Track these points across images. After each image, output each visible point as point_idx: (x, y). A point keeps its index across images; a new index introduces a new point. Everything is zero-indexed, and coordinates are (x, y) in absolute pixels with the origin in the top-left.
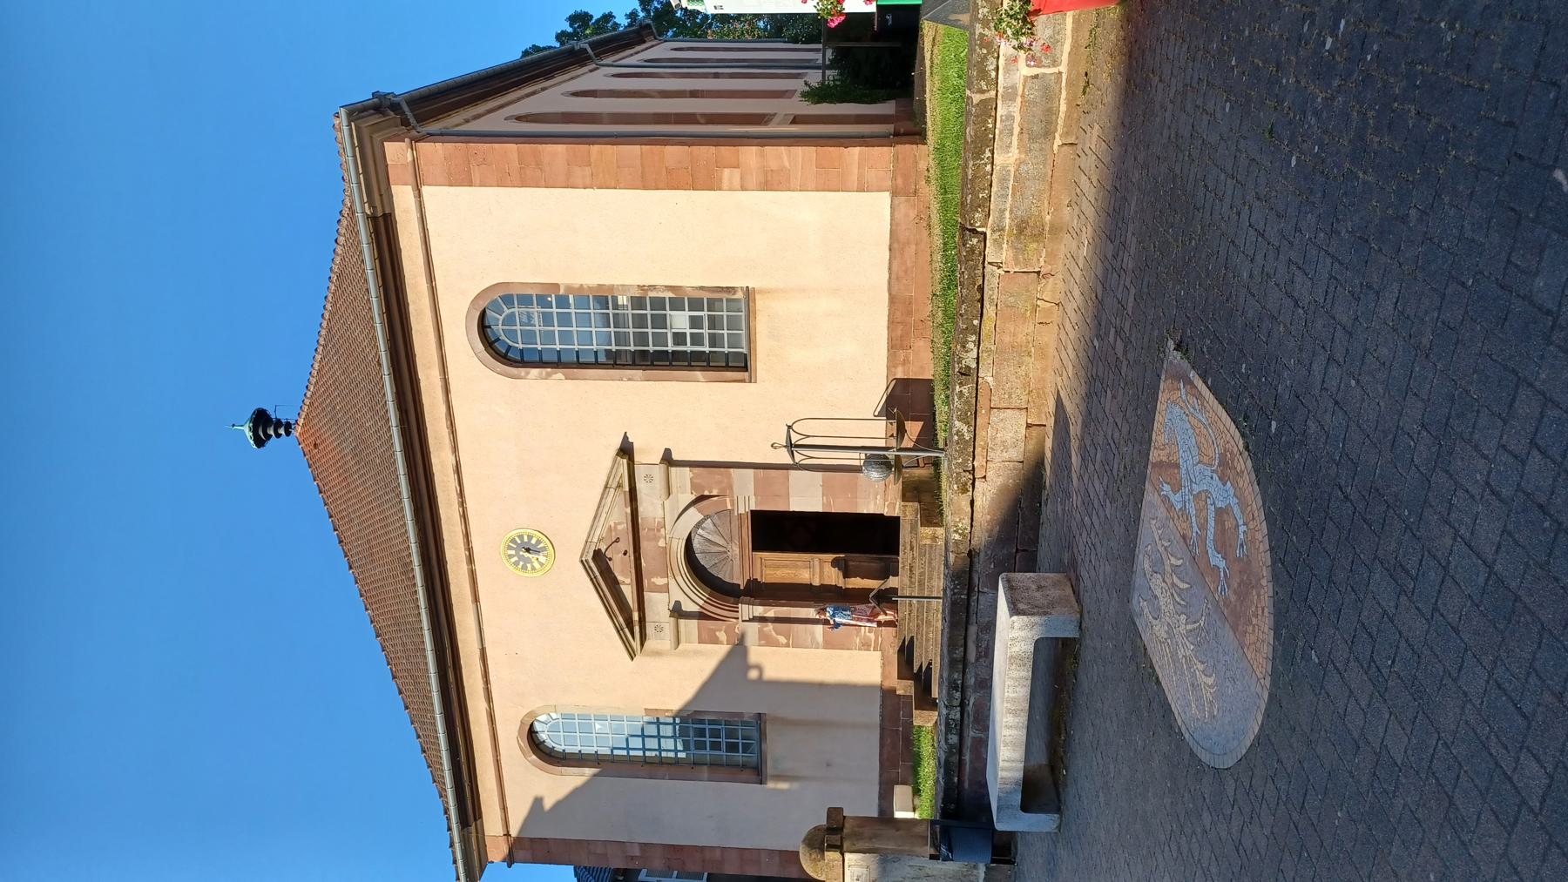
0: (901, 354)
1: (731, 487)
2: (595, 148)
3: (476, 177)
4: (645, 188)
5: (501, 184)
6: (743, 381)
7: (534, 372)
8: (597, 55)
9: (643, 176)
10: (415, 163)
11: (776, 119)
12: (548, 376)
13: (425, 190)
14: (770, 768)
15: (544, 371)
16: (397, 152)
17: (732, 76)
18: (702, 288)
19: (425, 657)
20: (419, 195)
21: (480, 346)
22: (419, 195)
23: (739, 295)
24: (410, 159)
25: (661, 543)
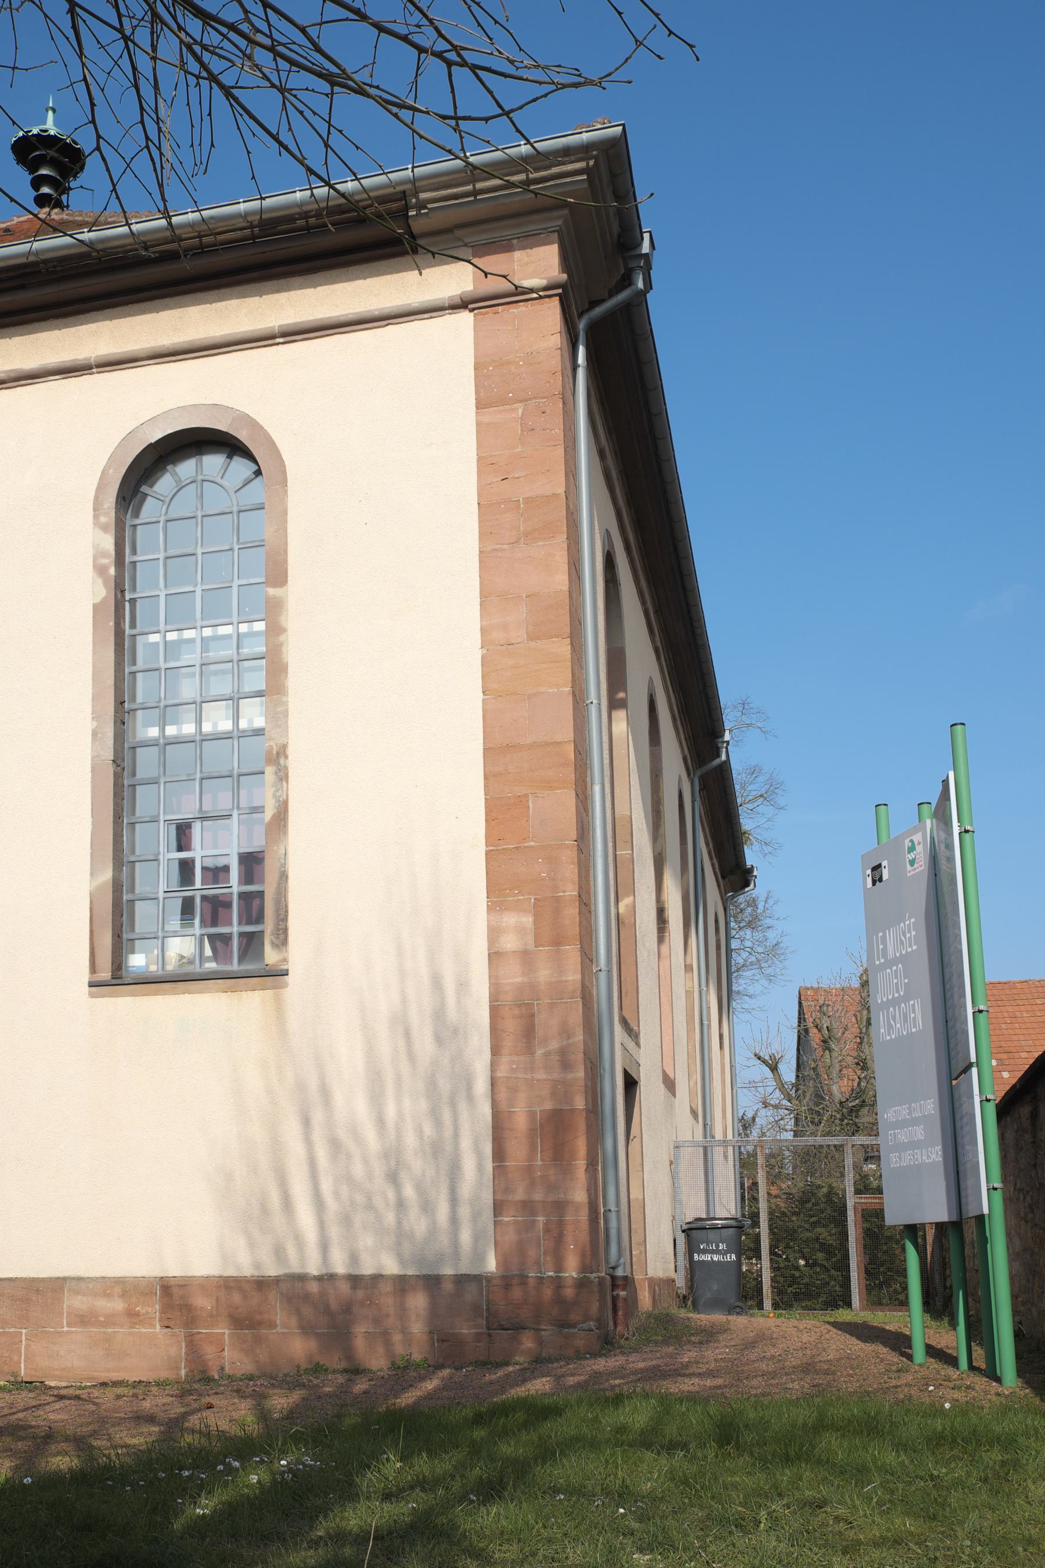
0: (153, 1309)
2: (561, 451)
3: (491, 416)
4: (488, 752)
5: (485, 464)
6: (93, 968)
7: (108, 542)
8: (703, 779)
9: (511, 748)
10: (519, 294)
11: (631, 1045)
12: (100, 570)
13: (465, 319)
15: (109, 561)
16: (540, 264)
17: (718, 942)
18: (284, 876)
19: (771, 1229)
20: (463, 304)
21: (156, 435)
22: (463, 304)
23: (271, 956)
24: (527, 283)
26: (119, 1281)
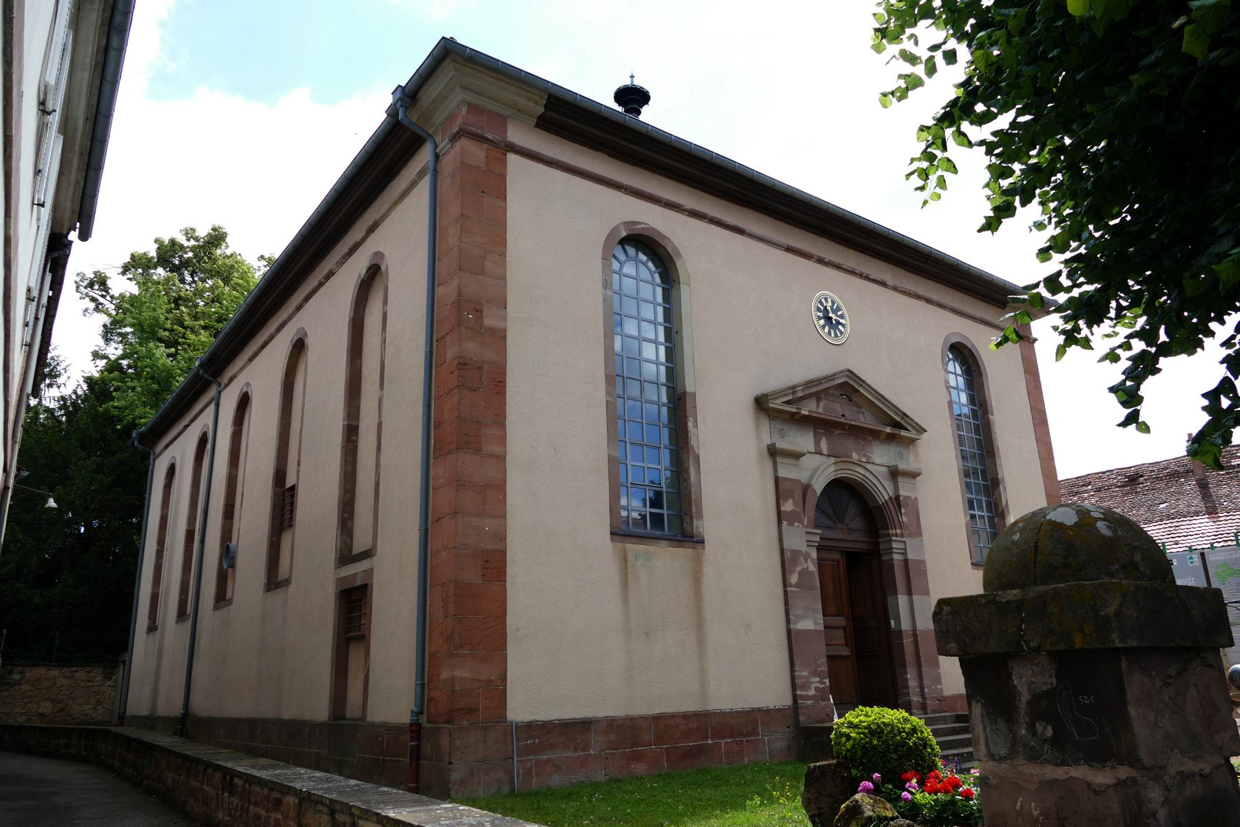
1: (911, 535)
14: (636, 549)
25: (855, 456)
26: (494, 565)
